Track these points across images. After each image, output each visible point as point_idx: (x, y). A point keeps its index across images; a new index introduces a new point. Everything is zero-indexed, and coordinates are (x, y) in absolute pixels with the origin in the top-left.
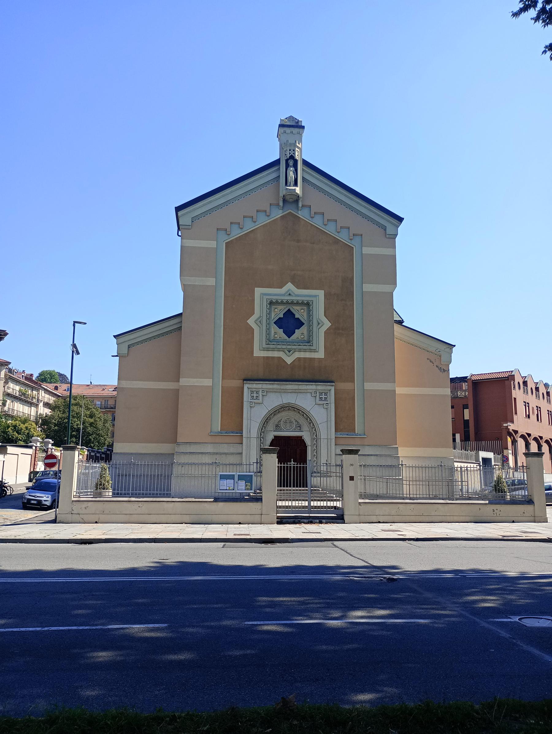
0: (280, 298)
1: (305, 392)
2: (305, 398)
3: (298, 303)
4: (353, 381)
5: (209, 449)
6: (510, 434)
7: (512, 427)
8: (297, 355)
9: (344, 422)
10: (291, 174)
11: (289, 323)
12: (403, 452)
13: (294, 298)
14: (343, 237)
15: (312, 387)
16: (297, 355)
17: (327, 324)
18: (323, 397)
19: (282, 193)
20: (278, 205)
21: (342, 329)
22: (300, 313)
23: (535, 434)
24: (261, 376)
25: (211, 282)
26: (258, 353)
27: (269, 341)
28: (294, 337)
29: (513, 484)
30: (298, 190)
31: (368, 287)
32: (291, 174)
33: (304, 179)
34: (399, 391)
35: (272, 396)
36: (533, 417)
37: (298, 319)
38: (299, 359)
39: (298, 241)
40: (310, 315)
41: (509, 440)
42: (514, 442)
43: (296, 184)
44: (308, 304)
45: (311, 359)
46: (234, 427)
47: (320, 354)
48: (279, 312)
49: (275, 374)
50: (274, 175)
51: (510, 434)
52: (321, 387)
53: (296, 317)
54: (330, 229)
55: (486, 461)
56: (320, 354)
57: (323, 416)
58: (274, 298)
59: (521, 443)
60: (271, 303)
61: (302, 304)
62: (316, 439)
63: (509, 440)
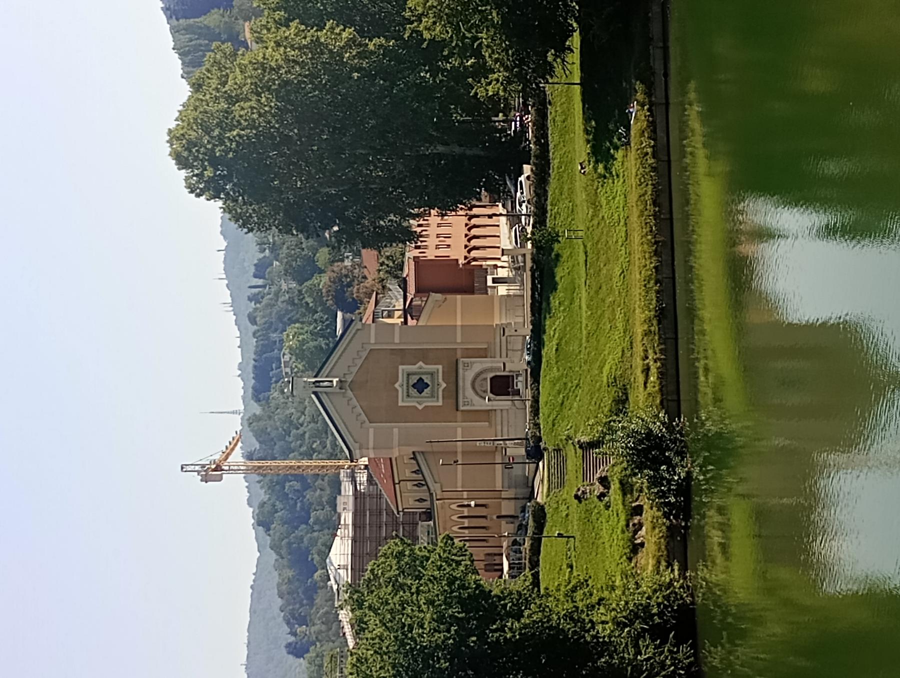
0: (405, 391)
1: (464, 375)
2: (467, 376)
3: (408, 381)
4: (456, 349)
5: (499, 428)
6: (469, 262)
7: (462, 261)
8: (440, 380)
9: (483, 354)
10: (326, 384)
11: (420, 386)
12: (497, 321)
13: (405, 382)
14: (364, 354)
15: (461, 371)
16: (440, 380)
17: (421, 363)
18: (467, 366)
19: (338, 390)
20: (344, 393)
21: (423, 355)
22: (414, 379)
23: (464, 241)
24: (454, 401)
25: (396, 430)
26: (440, 403)
27: (432, 396)
28: (429, 383)
29: (513, 262)
30: (335, 380)
31: (397, 340)
32: (326, 384)
33: (327, 377)
34: (459, 323)
35: (467, 394)
36: (448, 241)
37: (259, 551)
38: (443, 380)
39: (367, 381)
40: (414, 374)
41: (473, 263)
42: (475, 259)
43: (331, 381)
44: (408, 375)
45: (443, 372)
46: (487, 415)
47: (440, 367)
48: (414, 392)
49: (453, 392)
50: (324, 395)
51: (469, 262)
52: (461, 366)
53: (258, 554)
54: (359, 362)
55: (495, 281)
56: (440, 367)
57: (479, 365)
58: (405, 394)
59: (474, 254)
60: (408, 396)
61: (408, 378)
62: (491, 370)
63: (473, 263)
